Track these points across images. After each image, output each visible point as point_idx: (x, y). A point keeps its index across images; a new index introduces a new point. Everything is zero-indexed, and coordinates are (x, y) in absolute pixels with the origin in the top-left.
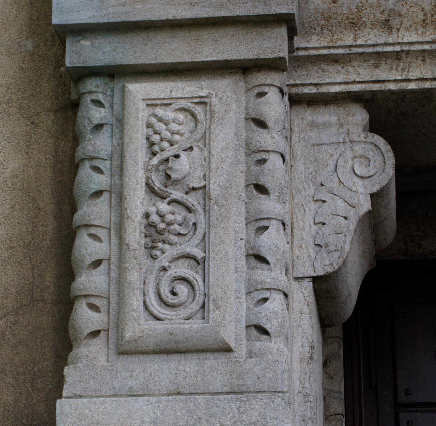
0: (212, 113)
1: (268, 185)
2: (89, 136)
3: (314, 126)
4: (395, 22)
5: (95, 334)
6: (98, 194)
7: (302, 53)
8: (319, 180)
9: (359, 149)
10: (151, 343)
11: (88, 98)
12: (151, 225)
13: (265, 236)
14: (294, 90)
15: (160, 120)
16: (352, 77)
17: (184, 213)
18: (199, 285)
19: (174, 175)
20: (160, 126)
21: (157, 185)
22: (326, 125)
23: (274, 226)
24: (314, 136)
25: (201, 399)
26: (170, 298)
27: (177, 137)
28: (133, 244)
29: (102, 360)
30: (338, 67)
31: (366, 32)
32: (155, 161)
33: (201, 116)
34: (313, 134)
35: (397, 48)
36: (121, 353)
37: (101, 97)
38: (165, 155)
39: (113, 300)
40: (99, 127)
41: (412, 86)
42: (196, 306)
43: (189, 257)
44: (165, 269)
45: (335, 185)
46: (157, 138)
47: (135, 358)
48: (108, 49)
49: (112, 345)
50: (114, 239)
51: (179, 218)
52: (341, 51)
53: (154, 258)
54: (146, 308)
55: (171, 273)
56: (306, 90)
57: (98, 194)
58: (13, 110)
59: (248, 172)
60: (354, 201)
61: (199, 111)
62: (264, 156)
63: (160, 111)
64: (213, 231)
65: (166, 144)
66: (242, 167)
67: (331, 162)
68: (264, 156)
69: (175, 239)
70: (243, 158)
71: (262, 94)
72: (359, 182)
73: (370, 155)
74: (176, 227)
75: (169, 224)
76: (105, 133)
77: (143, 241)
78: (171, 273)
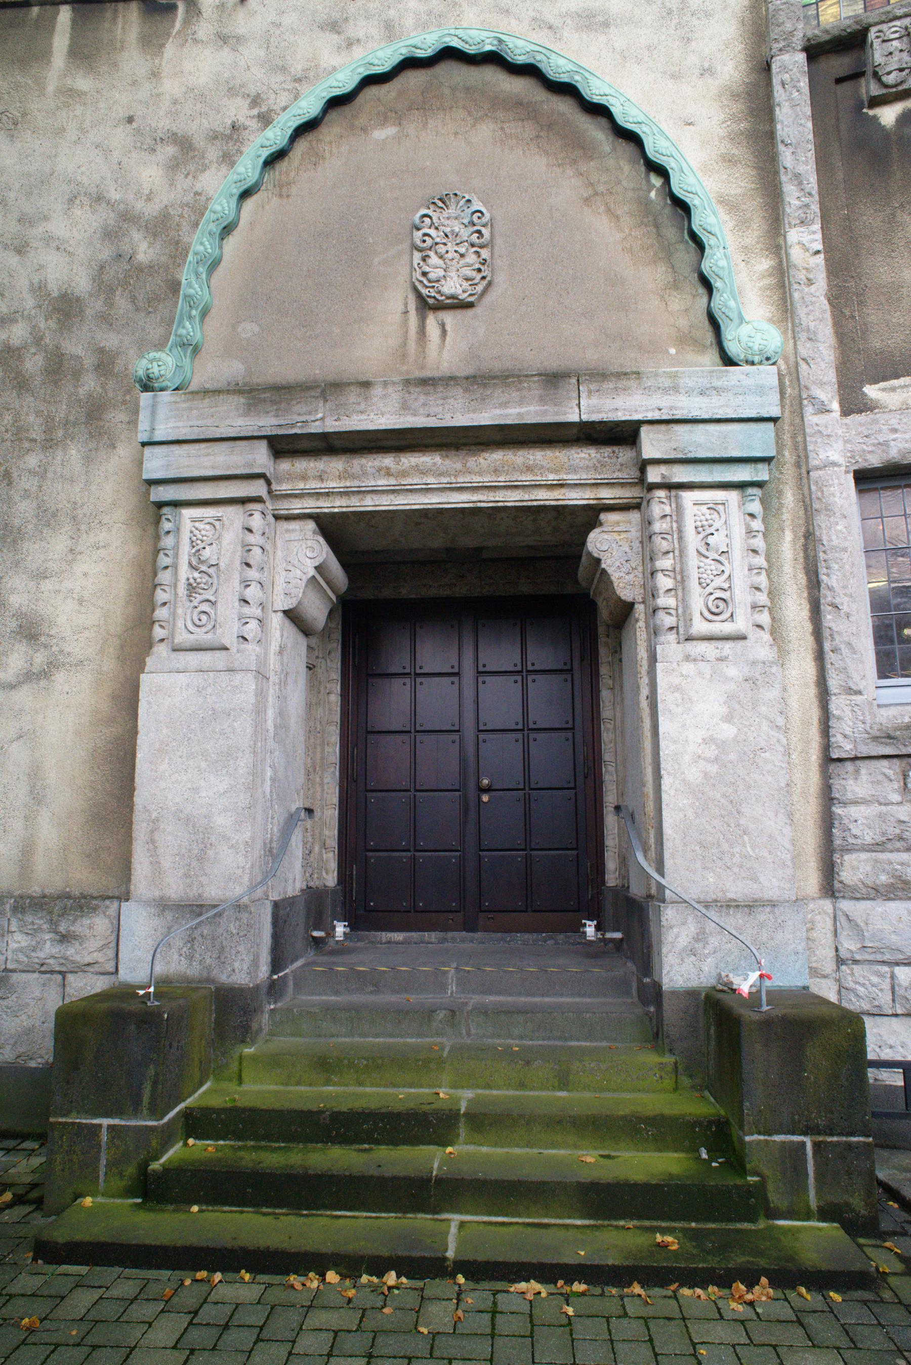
0: (223, 525)
1: (251, 563)
2: (163, 537)
3: (287, 531)
4: (325, 477)
5: (162, 640)
6: (166, 568)
7: (278, 493)
8: (289, 559)
9: (309, 543)
10: (187, 645)
11: (164, 518)
12: (190, 584)
13: (249, 589)
14: (276, 512)
15: (197, 529)
16: (306, 505)
17: (207, 578)
18: (213, 616)
19: (202, 558)
20: (196, 532)
21: (194, 563)
22: (294, 530)
23: (253, 584)
24: (287, 536)
25: (211, 674)
26: (198, 623)
27: (205, 538)
28: (180, 594)
29: (164, 654)
30: (298, 500)
31: (310, 481)
32: (193, 551)
33: (218, 527)
34: (286, 535)
35: (327, 490)
36: (174, 650)
37: (170, 517)
38: (198, 547)
39: (171, 623)
40: (168, 532)
41: (336, 510)
42: (210, 627)
43: (208, 601)
44: (196, 607)
45: (296, 562)
46: (194, 539)
47: (181, 653)
48: (172, 491)
49: (170, 646)
50: (173, 592)
51: (204, 581)
52: (298, 492)
53: (191, 601)
54: (186, 627)
55: (199, 609)
56: (282, 512)
57: (166, 568)
58: (133, 523)
59: (242, 557)
60: (305, 571)
61: (217, 524)
62: (250, 547)
63: (197, 524)
64: (220, 588)
65: (199, 542)
66: (239, 554)
67: (295, 550)
68: (250, 547)
69: (202, 591)
70: (240, 549)
71: (251, 515)
72: (308, 561)
73: (315, 546)
74: (202, 585)
75: (198, 584)
76: (171, 536)
77: (186, 593)
78: (199, 609)
